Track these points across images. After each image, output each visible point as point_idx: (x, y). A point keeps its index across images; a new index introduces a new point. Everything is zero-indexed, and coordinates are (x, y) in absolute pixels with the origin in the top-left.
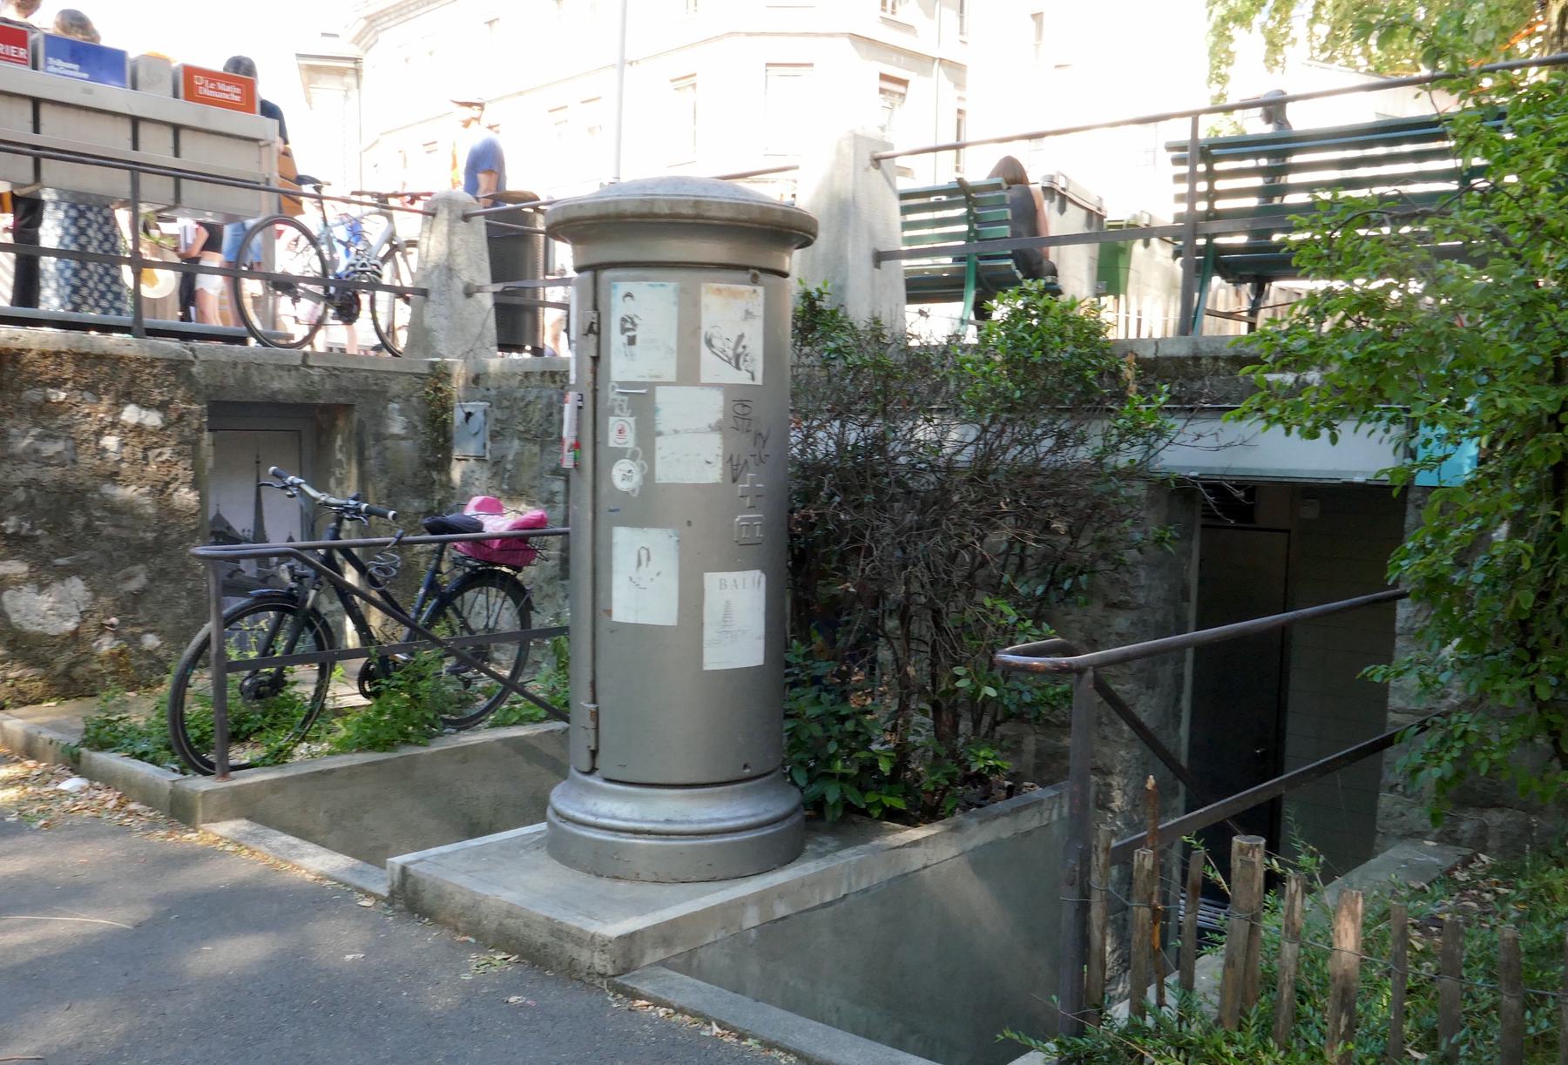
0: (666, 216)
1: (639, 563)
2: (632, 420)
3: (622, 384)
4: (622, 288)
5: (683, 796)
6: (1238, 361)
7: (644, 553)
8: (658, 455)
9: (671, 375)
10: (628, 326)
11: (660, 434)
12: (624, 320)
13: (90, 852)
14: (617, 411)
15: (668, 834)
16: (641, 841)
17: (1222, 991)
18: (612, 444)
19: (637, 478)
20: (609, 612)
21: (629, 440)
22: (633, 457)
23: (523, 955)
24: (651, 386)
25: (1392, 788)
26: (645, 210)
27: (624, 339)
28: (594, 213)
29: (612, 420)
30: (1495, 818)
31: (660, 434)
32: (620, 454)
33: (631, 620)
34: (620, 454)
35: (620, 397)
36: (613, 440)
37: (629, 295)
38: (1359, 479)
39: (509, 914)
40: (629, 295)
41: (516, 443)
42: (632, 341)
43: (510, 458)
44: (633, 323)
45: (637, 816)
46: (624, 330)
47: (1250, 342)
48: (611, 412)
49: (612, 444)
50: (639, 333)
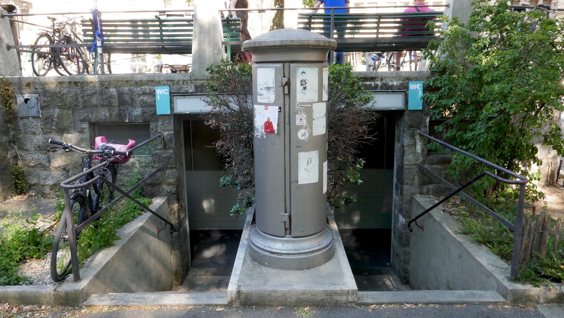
0: (323, 46)
1: (308, 164)
2: (305, 116)
3: (301, 103)
4: (301, 70)
5: (313, 238)
6: (365, 79)
7: (309, 160)
8: (313, 126)
9: (316, 100)
10: (304, 83)
11: (314, 119)
12: (301, 81)
13: (473, 295)
14: (299, 113)
15: (281, 254)
16: (290, 257)
17: (51, 269)
18: (297, 124)
19: (307, 135)
20: (297, 182)
21: (304, 122)
22: (306, 128)
23: (310, 306)
24: (311, 103)
25: (407, 184)
26: (317, 44)
27: (302, 88)
28: (298, 44)
29: (297, 116)
30: (431, 186)
31: (314, 119)
32: (300, 127)
33: (306, 183)
34: (300, 127)
35: (300, 108)
36: (298, 123)
37: (303, 72)
38: (394, 109)
39: (303, 294)
40: (303, 72)
41: (57, 110)
42: (305, 88)
43: (56, 116)
44: (305, 82)
45: (291, 248)
46: (302, 85)
47: (392, 78)
48: (297, 113)
49: (297, 124)
50: (307, 85)
